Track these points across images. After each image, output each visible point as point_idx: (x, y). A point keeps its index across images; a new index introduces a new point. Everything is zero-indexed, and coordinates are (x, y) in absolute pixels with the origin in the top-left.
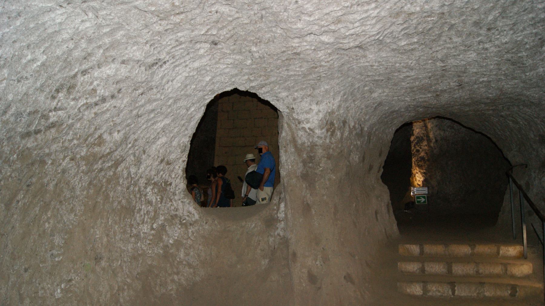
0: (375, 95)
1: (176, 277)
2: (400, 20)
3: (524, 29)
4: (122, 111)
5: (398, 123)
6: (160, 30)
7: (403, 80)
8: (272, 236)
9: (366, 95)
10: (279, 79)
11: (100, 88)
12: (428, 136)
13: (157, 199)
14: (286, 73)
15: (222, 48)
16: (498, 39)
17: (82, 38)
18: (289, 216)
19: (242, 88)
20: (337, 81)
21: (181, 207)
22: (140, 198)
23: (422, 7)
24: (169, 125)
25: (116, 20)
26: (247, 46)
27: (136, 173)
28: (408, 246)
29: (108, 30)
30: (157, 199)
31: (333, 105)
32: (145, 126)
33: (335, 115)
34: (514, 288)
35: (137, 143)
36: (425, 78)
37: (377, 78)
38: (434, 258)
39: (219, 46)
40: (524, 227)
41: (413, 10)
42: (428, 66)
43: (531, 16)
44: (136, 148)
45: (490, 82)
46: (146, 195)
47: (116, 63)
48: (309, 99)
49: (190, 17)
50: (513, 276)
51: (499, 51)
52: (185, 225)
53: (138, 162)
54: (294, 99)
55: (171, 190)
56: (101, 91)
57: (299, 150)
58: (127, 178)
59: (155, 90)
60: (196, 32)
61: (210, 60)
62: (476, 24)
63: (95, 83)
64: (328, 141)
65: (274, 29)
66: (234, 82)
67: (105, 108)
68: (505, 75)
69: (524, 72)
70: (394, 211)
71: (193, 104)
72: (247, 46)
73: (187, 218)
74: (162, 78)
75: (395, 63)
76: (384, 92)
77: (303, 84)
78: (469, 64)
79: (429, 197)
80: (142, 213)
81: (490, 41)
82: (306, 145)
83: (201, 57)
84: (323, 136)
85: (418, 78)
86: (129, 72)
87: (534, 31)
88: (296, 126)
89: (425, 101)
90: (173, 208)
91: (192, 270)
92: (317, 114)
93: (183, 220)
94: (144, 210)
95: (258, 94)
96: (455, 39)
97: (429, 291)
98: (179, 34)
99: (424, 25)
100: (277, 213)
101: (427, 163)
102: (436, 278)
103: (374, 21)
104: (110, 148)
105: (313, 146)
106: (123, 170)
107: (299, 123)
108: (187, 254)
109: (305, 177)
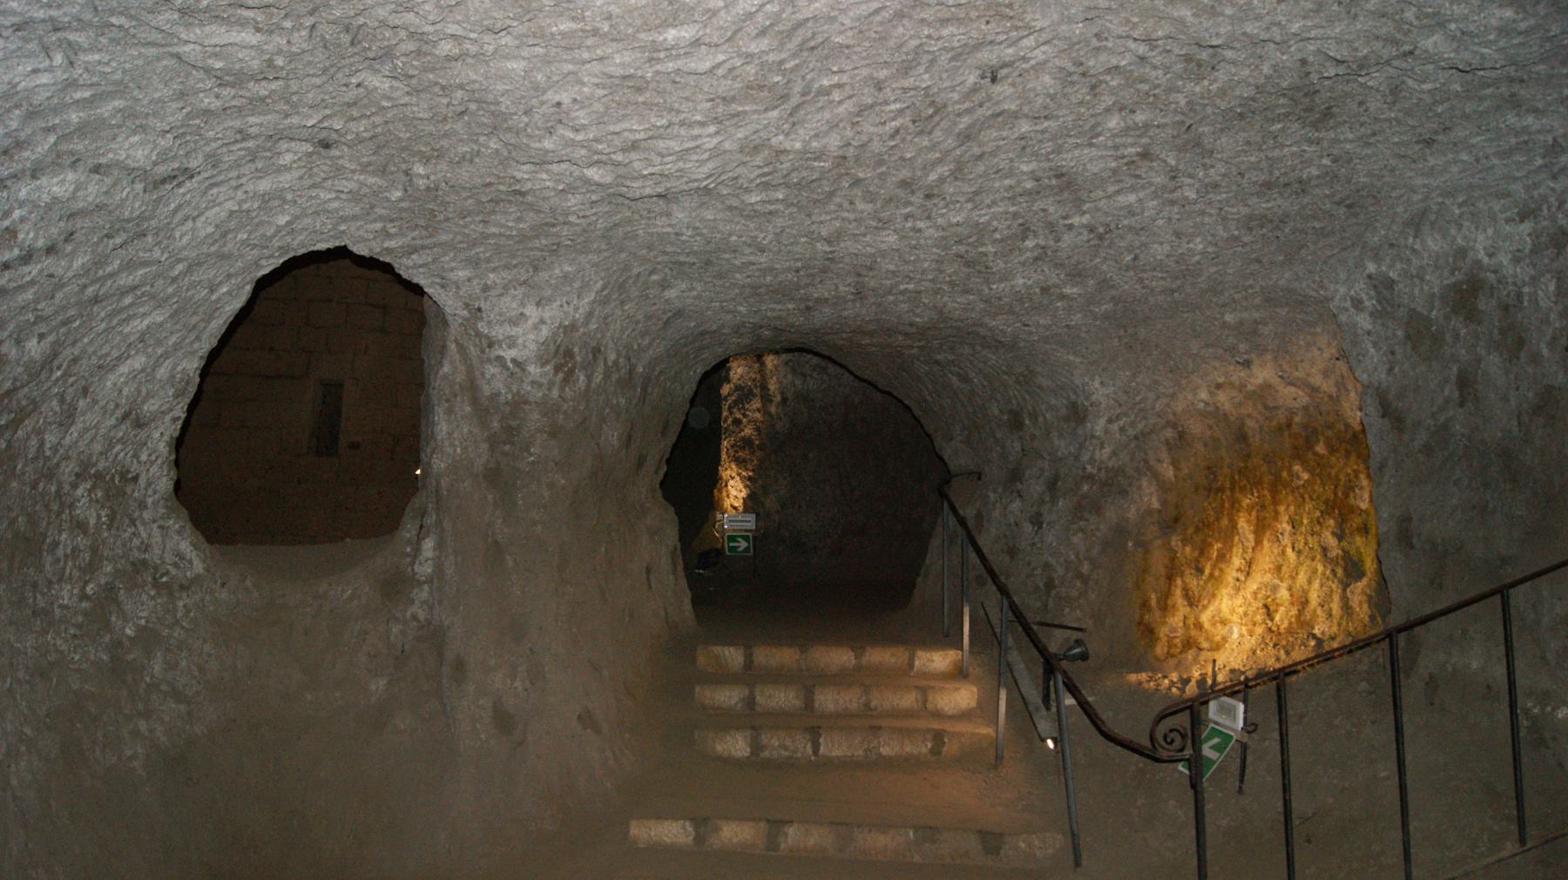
0: (671, 293)
1: (142, 725)
2: (759, 160)
3: (994, 203)
4: (63, 286)
5: (709, 358)
6: (212, 107)
7: (739, 269)
8: (397, 620)
9: (652, 292)
10: (459, 238)
11: (26, 226)
12: (764, 387)
13: (99, 517)
14: (480, 228)
15: (341, 157)
16: (943, 215)
17: (16, 107)
18: (450, 571)
19: (360, 249)
20: (594, 258)
21: (159, 539)
22: (59, 514)
23: (806, 143)
24: (161, 325)
25: (118, 76)
26: (405, 161)
27: (55, 449)
28: (717, 650)
29: (87, 94)
30: (99, 517)
31: (576, 309)
32: (103, 325)
33: (577, 335)
34: (938, 737)
35: (75, 369)
36: (789, 270)
37: (682, 258)
38: (778, 677)
39: (334, 152)
40: (966, 610)
41: (787, 145)
42: (798, 249)
43: (1007, 182)
44: (72, 380)
45: (920, 292)
46: (72, 506)
47: (81, 169)
48: (520, 292)
49: (294, 88)
50: (938, 715)
51: (944, 238)
52: (168, 590)
53: (68, 417)
54: (486, 288)
55: (136, 494)
56: (26, 236)
57: (482, 411)
58: (36, 458)
59: (150, 239)
60: (295, 120)
61: (301, 178)
62: (904, 184)
63: (17, 214)
64: (555, 393)
65: (482, 139)
66: (343, 232)
67: (28, 279)
68: (950, 283)
69: (987, 282)
70: (686, 568)
71: (229, 276)
72: (405, 161)
73: (173, 571)
74: (175, 211)
75: (730, 235)
76: (692, 289)
77: (514, 256)
78: (883, 254)
79: (759, 539)
80: (60, 552)
81: (929, 218)
82: (502, 399)
83: (287, 168)
84: (544, 381)
85: (772, 269)
86: (106, 193)
87: (1012, 209)
88: (483, 351)
89: (780, 318)
90: (136, 542)
91: (182, 707)
92: (536, 327)
93: (163, 575)
94: (65, 547)
95: (396, 266)
96: (860, 206)
97: (763, 748)
98: (252, 120)
99: (804, 174)
100: (413, 564)
101: (758, 454)
102: (781, 720)
103: (706, 156)
104: (15, 379)
105: (519, 402)
106: (28, 438)
107: (490, 346)
108: (171, 666)
109: (493, 476)
